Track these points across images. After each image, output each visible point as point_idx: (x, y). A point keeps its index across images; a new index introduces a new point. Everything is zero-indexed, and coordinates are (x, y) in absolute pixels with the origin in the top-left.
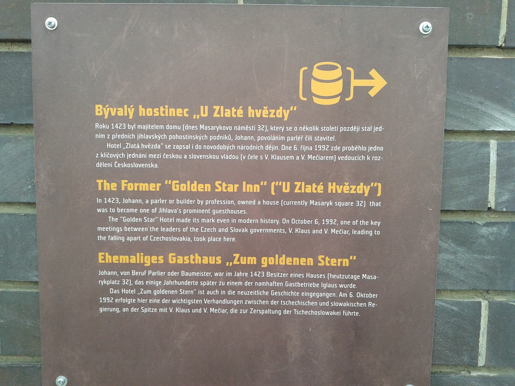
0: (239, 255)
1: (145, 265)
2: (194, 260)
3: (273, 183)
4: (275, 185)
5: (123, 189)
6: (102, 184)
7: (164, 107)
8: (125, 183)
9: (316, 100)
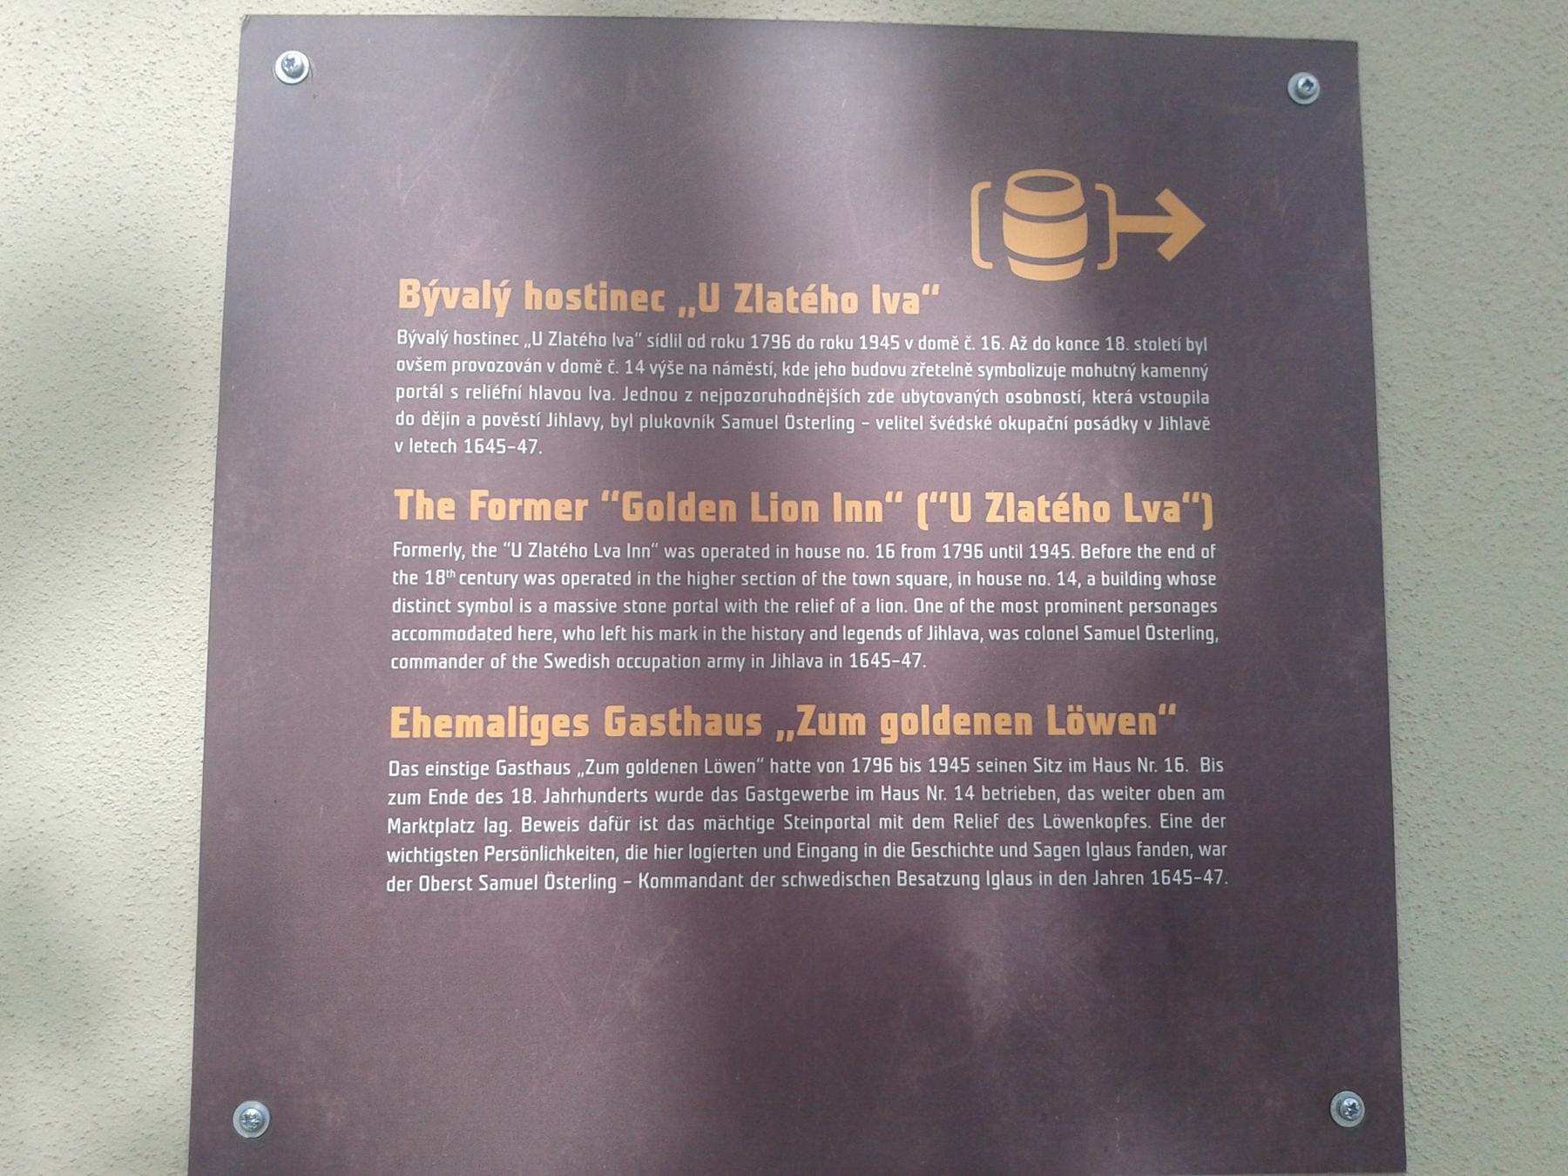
0: (813, 707)
1: (534, 743)
2: (680, 725)
3: (922, 498)
4: (928, 501)
5: (474, 516)
6: (412, 501)
7: (596, 287)
8: (482, 499)
9: (1017, 268)
